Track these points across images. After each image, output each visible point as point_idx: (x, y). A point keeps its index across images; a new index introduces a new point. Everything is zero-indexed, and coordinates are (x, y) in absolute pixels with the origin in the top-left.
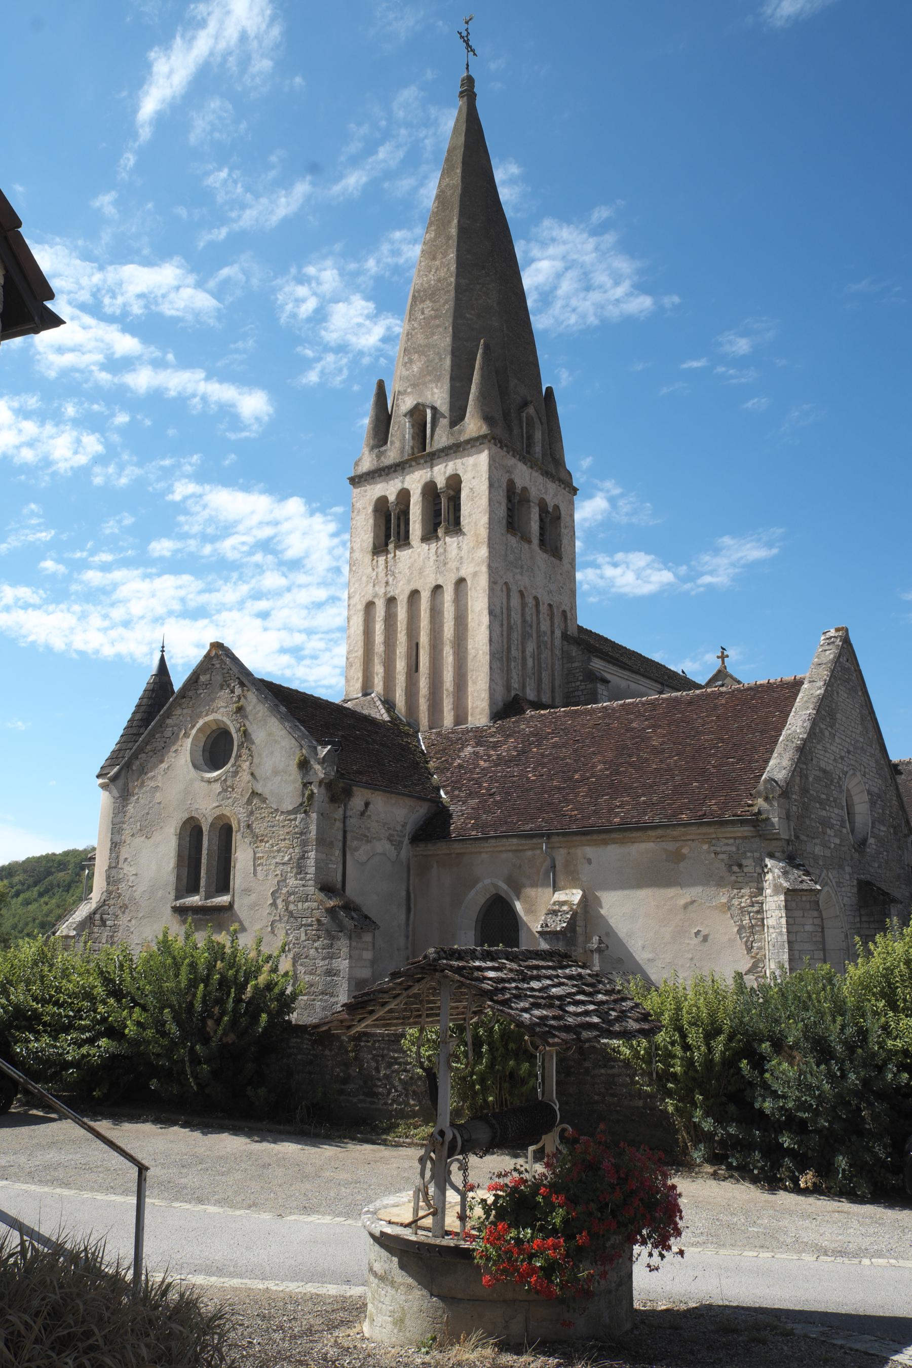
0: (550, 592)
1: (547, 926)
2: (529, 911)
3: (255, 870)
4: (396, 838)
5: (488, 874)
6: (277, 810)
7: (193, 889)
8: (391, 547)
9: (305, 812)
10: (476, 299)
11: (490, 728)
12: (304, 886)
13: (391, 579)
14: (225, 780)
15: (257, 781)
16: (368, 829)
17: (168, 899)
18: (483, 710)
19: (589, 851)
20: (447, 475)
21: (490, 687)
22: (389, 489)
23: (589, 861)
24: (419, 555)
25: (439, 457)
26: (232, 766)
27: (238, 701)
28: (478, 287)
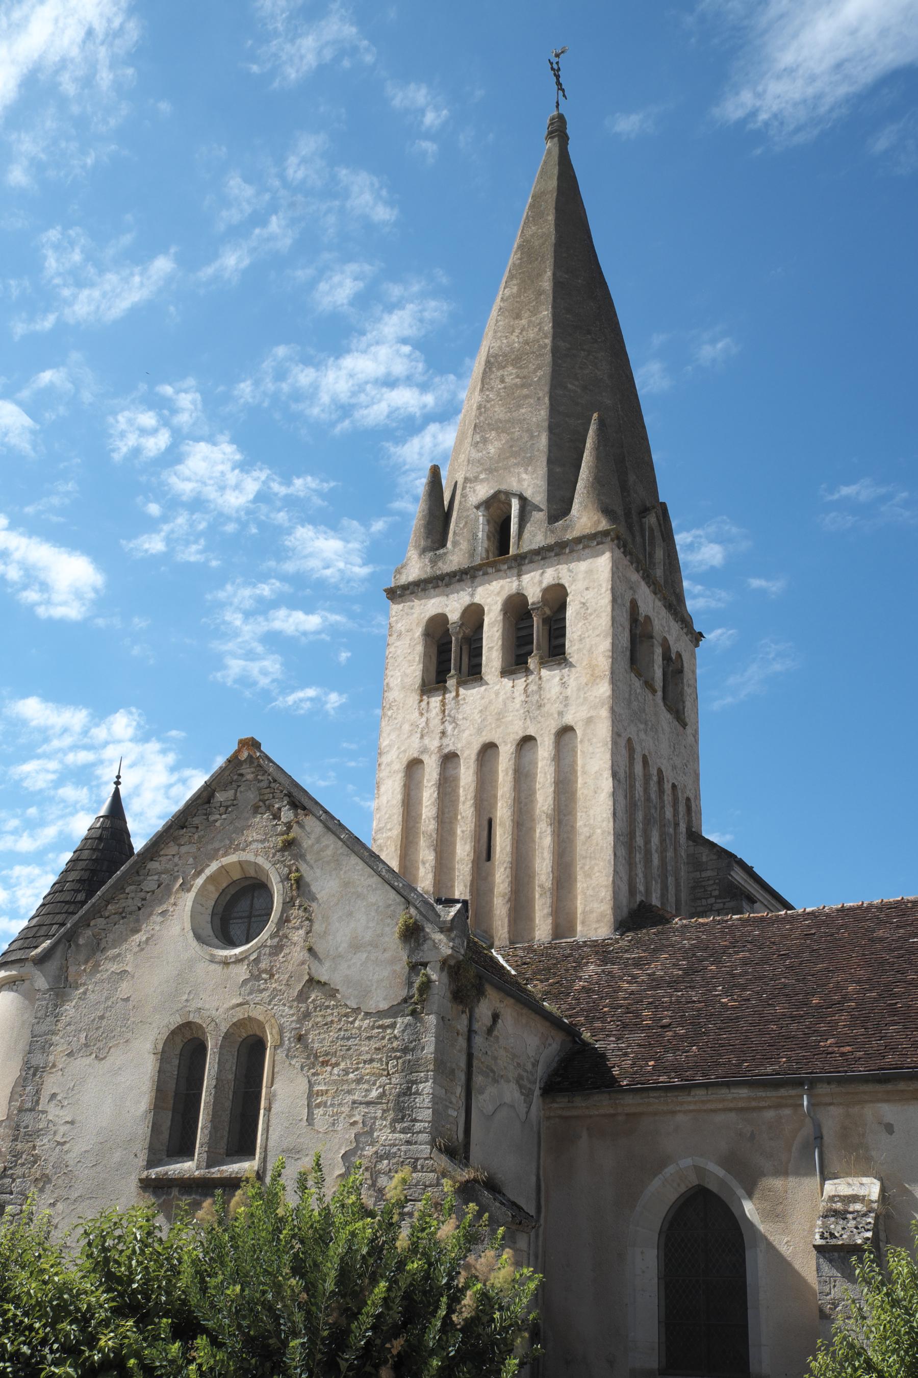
0: (674, 767)
1: (832, 1235)
2: (766, 1215)
3: (310, 1115)
4: (525, 1082)
5: (687, 1146)
6: (357, 1010)
7: (182, 1147)
8: (451, 683)
9: (413, 1013)
10: (581, 368)
11: (617, 941)
12: (408, 1142)
13: (449, 728)
14: (257, 961)
15: (320, 960)
17: (136, 1168)
18: (602, 915)
19: (888, 1111)
20: (544, 585)
21: (614, 882)
22: (452, 606)
23: (890, 1129)
24: (497, 694)
25: (531, 562)
26: (272, 937)
27: (287, 832)
28: (583, 354)
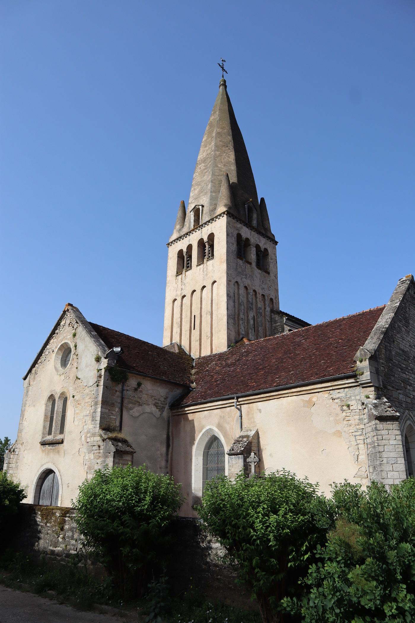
0: (263, 289)
1: (233, 450)
7: (50, 433)
16: (140, 398)
23: (260, 411)
